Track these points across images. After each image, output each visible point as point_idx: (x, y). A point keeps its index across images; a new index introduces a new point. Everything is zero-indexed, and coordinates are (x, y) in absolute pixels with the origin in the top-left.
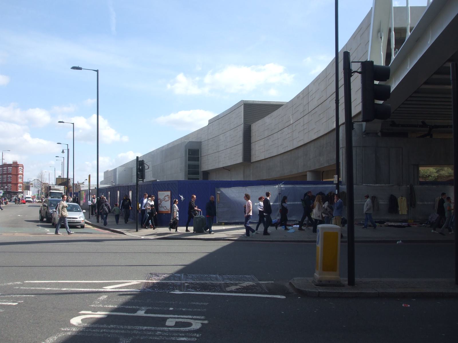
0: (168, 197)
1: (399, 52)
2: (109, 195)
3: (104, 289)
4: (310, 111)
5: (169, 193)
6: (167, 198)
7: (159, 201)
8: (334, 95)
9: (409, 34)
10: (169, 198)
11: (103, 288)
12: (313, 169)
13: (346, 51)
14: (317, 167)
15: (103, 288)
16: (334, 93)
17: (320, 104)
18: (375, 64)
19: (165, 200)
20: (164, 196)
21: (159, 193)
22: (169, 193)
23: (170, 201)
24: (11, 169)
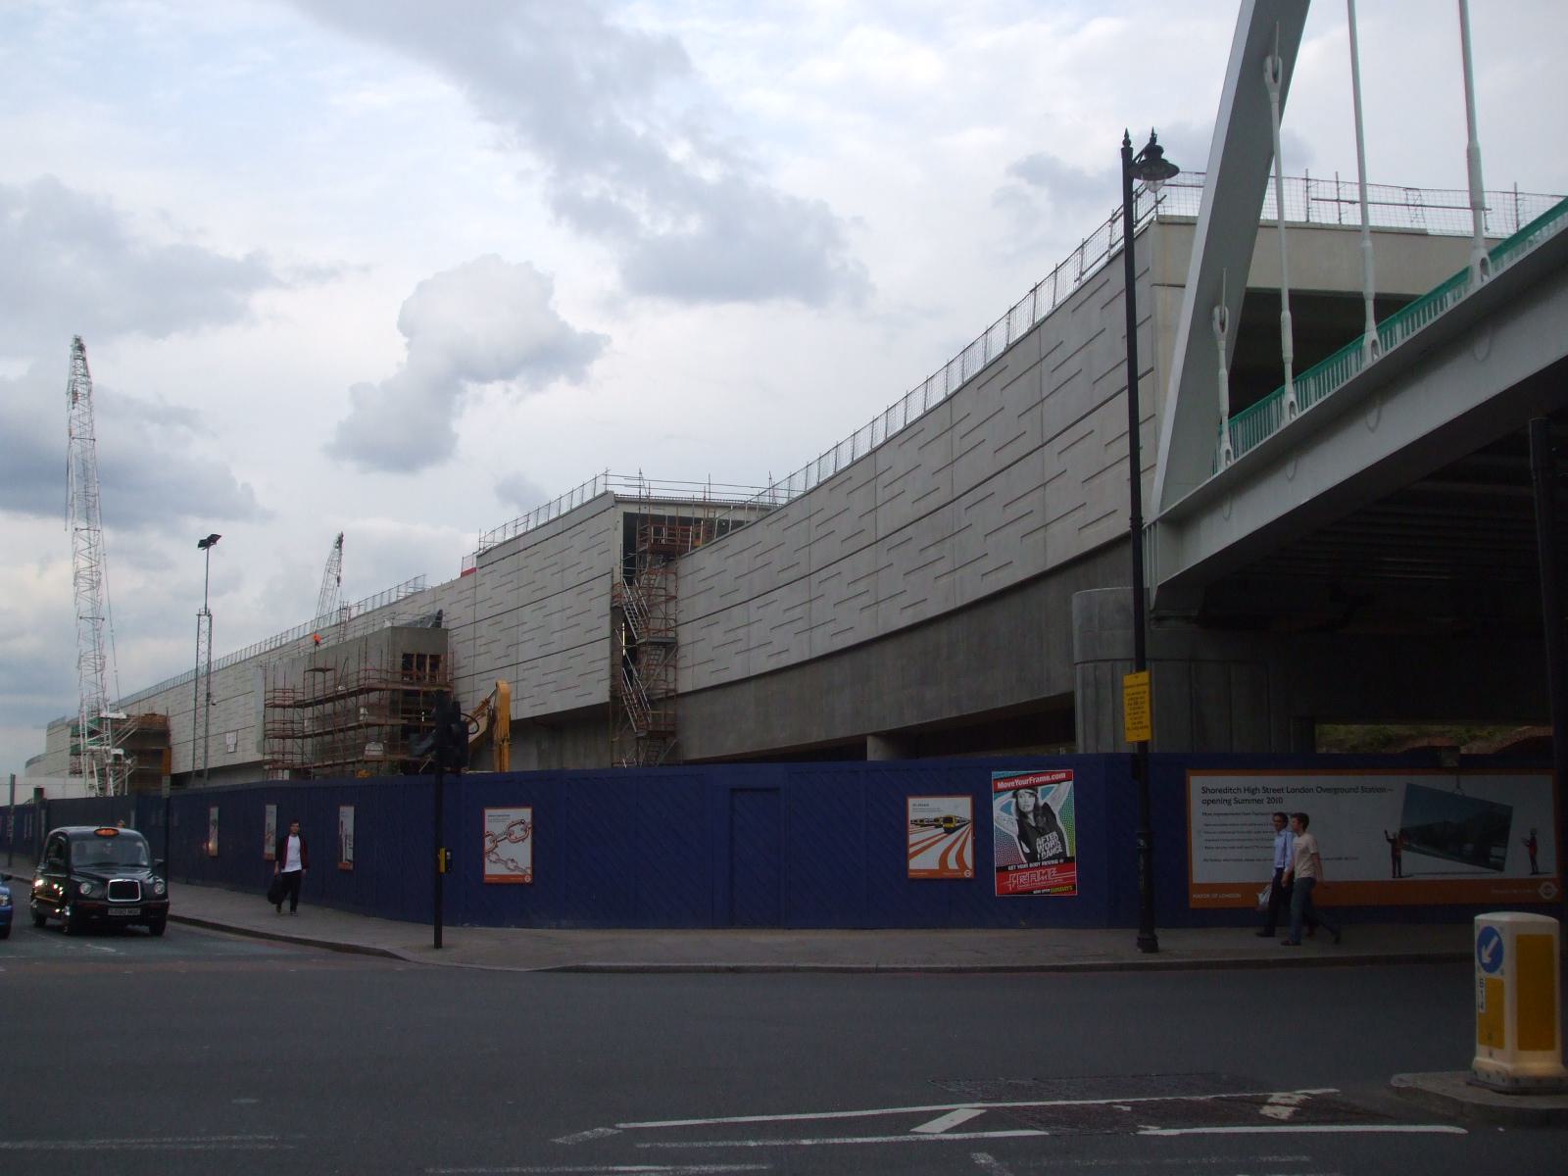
0: (522, 826)
1: (1246, 454)
2: (213, 831)
3: (916, 1133)
4: (881, 535)
5: (525, 814)
6: (518, 831)
7: (487, 840)
8: (1125, 367)
9: (1102, 29)
10: (526, 831)
11: (912, 1130)
12: (892, 724)
13: (1304, 812)
14: (911, 719)
15: (912, 1130)
16: (1142, 323)
17: (925, 513)
18: (1163, 156)
19: (513, 837)
20: (508, 822)
21: (488, 812)
22: (525, 814)
23: (529, 841)
24: (122, 794)
